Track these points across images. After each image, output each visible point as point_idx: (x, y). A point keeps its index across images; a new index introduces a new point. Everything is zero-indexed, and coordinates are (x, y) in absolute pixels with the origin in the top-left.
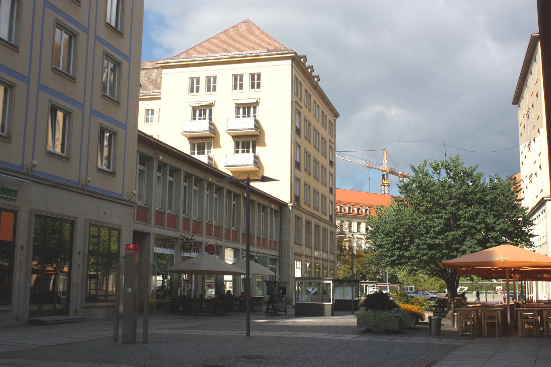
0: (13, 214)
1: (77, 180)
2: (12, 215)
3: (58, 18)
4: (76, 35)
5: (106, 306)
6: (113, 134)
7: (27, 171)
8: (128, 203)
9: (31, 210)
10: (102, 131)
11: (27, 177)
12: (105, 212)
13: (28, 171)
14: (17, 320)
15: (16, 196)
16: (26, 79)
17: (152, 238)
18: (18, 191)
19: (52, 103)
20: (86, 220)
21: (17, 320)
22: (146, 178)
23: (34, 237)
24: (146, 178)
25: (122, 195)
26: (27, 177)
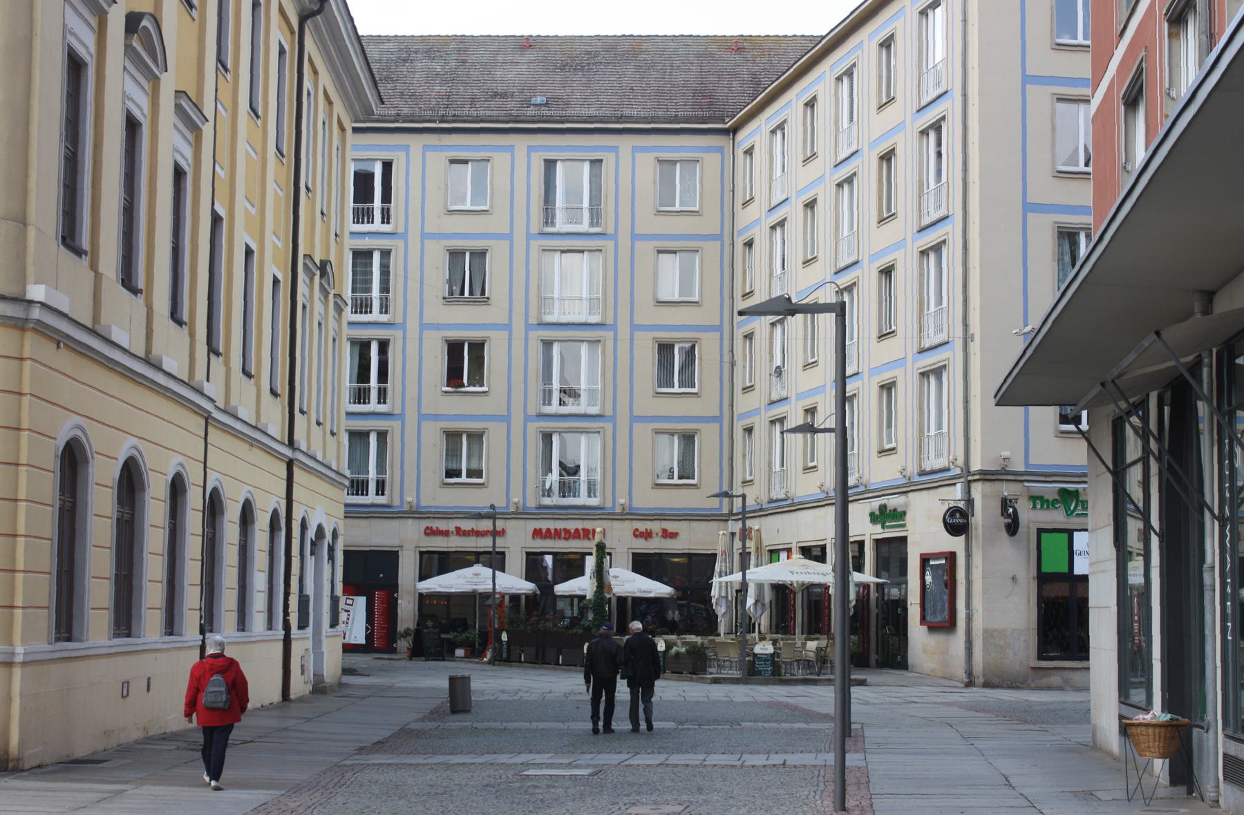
23: (541, 530)
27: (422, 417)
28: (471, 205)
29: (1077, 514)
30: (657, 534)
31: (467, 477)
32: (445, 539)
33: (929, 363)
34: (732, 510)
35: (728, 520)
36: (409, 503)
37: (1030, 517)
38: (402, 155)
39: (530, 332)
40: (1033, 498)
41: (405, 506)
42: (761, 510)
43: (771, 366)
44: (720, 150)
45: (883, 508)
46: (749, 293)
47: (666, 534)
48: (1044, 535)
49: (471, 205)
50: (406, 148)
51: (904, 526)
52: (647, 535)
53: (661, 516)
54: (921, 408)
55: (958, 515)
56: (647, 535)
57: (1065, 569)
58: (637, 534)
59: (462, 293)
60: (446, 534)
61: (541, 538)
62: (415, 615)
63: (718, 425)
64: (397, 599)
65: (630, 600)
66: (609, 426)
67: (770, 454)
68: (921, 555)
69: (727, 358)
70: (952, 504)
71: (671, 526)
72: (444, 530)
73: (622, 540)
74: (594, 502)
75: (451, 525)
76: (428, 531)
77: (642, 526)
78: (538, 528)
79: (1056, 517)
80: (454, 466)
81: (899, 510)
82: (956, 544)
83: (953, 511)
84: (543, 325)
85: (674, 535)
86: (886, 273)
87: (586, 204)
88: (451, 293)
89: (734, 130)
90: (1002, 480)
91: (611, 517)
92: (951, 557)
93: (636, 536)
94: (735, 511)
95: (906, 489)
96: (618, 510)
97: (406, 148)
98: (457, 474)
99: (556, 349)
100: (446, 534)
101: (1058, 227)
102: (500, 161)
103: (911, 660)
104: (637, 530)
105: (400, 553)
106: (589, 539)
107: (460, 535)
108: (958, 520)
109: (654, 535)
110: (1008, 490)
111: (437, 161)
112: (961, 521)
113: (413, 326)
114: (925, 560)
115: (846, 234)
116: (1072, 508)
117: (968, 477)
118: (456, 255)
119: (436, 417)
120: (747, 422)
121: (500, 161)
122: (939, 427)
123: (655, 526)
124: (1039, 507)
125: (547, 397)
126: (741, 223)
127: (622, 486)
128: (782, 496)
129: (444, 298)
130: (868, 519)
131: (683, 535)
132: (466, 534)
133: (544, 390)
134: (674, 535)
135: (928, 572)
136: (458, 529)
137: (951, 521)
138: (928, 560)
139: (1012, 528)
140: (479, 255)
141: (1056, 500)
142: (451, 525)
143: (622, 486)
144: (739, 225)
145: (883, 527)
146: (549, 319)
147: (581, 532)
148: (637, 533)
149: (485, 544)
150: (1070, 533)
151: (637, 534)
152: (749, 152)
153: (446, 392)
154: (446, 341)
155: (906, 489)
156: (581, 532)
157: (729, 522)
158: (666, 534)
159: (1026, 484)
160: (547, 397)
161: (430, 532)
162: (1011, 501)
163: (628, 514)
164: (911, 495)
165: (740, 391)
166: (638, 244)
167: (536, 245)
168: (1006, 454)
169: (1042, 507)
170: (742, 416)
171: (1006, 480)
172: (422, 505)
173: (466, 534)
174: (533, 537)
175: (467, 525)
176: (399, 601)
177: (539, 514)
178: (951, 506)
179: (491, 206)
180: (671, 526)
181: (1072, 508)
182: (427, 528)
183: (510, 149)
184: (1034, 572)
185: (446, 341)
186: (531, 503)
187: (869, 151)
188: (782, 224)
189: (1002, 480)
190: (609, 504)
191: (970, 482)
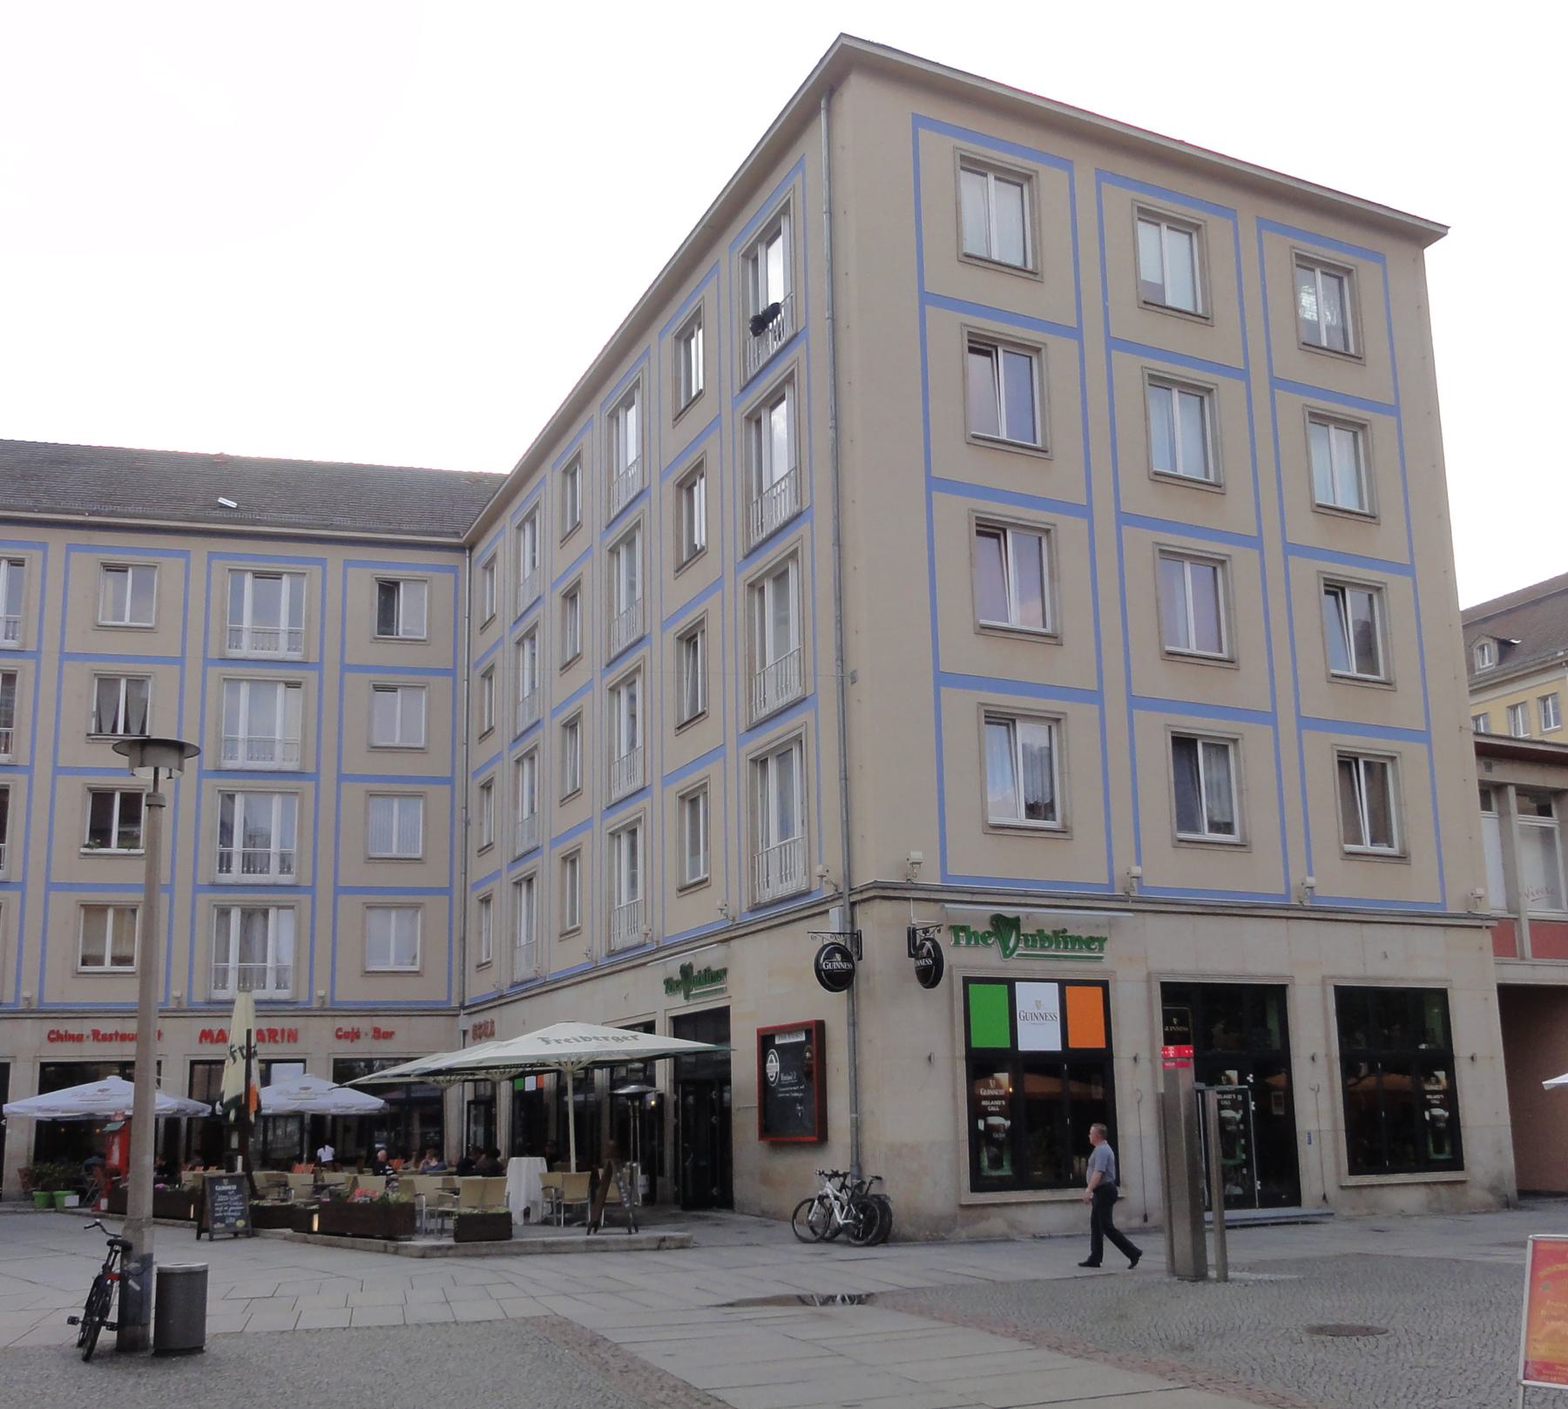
0: (1100, 989)
1: (1282, 890)
2: (1099, 991)
3: (1161, 541)
4: (1031, 177)
5: (1426, 1184)
6: (1377, 771)
7: (1126, 893)
8: (1470, 921)
9: (1149, 974)
10: (1347, 763)
11: (1123, 906)
12: (1385, 953)
13: (1127, 890)
14: (1146, 1218)
15: (1101, 949)
16: (1269, 718)
17: (23, 1077)
18: (1105, 939)
19: (1339, 748)
20: (1324, 978)
21: (1146, 1218)
22: (640, 1195)
23: (210, 1032)
24: (640, 1195)
25: (1287, 896)
26: (1123, 906)
27: (51, 887)
28: (131, 621)
29: (1019, 955)
30: (366, 1034)
31: (112, 965)
32: (77, 1045)
33: (777, 735)
34: (464, 1001)
35: (458, 1015)
36: (27, 999)
37: (959, 959)
38: (38, 554)
39: (204, 780)
40: (957, 930)
41: (21, 1003)
42: (501, 997)
43: (456, 1247)
44: (453, 569)
45: (686, 971)
46: (487, 846)
47: (379, 1034)
48: (971, 986)
49: (131, 621)
50: (44, 546)
51: (722, 991)
52: (354, 1035)
53: (371, 1011)
54: (753, 813)
55: (838, 956)
56: (354, 1035)
57: (1005, 1043)
58: (340, 1035)
59: (114, 729)
60: (79, 1038)
61: (211, 1042)
62: (29, 1149)
63: (446, 898)
64: (5, 1127)
65: (330, 1117)
66: (305, 899)
67: (514, 924)
68: (758, 1031)
69: (459, 814)
70: (828, 939)
71: (384, 1024)
72: (76, 1033)
73: (320, 1040)
74: (284, 994)
75: (85, 1027)
76: (53, 1036)
77: (347, 1024)
78: (207, 1029)
79: (988, 960)
80: (92, 951)
81: (715, 968)
82: (829, 1007)
83: (835, 949)
84: (220, 772)
85: (388, 1035)
86: (689, 641)
87: (284, 623)
88: (100, 729)
89: (470, 547)
90: (907, 899)
91: (307, 1013)
92: (816, 1031)
93: (339, 1037)
94: (467, 1004)
95: (728, 935)
96: (315, 1005)
97: (44, 546)
98: (99, 961)
99: (239, 801)
100: (79, 1038)
101: (977, 518)
102: (171, 569)
103: (738, 1193)
104: (340, 1029)
105: (12, 1066)
106: (276, 1042)
107: (98, 1040)
108: (838, 963)
109: (362, 1035)
110: (919, 915)
111: (86, 566)
112: (844, 966)
113: (43, 769)
114: (766, 1040)
115: (623, 608)
116: (1011, 945)
117: (855, 899)
118: (107, 683)
119: (70, 887)
120: (483, 891)
121: (171, 569)
122: (785, 830)
123: (364, 1025)
124: (963, 942)
125: (225, 862)
126: (475, 875)
127: (322, 972)
128: (531, 975)
129: (89, 735)
130: (663, 987)
131: (400, 1036)
132: (107, 1038)
133: (222, 855)
134: (388, 1035)
135: (771, 1057)
136: (96, 1034)
137: (829, 967)
138: (772, 1037)
139: (930, 975)
140: (137, 682)
141: (988, 932)
142: (85, 1027)
143: (322, 972)
144: (473, 877)
145: (687, 997)
146: (229, 764)
147: (266, 1034)
148: (340, 1033)
149: (126, 1051)
150: (1010, 983)
151: (340, 1035)
152: (489, 567)
153: (86, 854)
154: (90, 790)
155: (728, 935)
156: (266, 1034)
157: (460, 1017)
158: (379, 1034)
159: (947, 905)
160: (225, 862)
161: (56, 1037)
162: (926, 931)
163: (330, 1010)
164: (733, 943)
165: (474, 968)
166: (349, 676)
167: (215, 672)
168: (916, 855)
169: (968, 943)
170: (476, 886)
171: (915, 899)
172: (46, 1001)
173: (107, 1038)
174: (201, 1041)
175: (107, 1027)
176: (8, 1131)
177: (209, 1011)
178: (826, 942)
179: (157, 621)
180: (384, 1024)
181: (1011, 945)
182: (52, 1032)
183: (185, 554)
184: (961, 1051)
185: (90, 790)
186: (199, 998)
187: (550, 849)
188: (530, 635)
189: (907, 899)
190: (303, 998)
191: (853, 904)
